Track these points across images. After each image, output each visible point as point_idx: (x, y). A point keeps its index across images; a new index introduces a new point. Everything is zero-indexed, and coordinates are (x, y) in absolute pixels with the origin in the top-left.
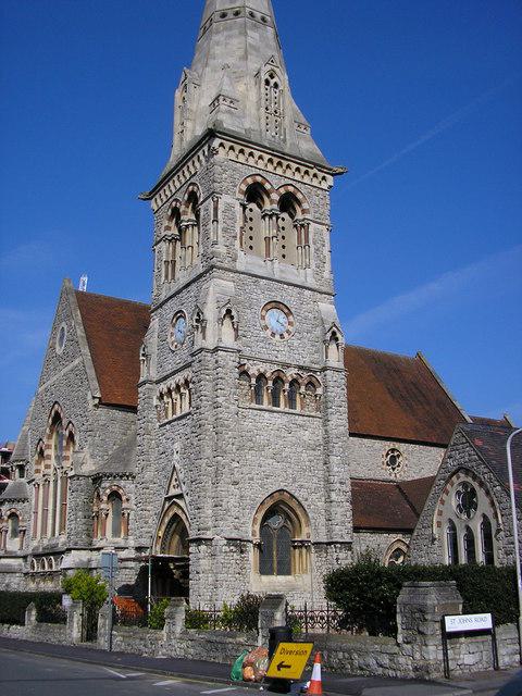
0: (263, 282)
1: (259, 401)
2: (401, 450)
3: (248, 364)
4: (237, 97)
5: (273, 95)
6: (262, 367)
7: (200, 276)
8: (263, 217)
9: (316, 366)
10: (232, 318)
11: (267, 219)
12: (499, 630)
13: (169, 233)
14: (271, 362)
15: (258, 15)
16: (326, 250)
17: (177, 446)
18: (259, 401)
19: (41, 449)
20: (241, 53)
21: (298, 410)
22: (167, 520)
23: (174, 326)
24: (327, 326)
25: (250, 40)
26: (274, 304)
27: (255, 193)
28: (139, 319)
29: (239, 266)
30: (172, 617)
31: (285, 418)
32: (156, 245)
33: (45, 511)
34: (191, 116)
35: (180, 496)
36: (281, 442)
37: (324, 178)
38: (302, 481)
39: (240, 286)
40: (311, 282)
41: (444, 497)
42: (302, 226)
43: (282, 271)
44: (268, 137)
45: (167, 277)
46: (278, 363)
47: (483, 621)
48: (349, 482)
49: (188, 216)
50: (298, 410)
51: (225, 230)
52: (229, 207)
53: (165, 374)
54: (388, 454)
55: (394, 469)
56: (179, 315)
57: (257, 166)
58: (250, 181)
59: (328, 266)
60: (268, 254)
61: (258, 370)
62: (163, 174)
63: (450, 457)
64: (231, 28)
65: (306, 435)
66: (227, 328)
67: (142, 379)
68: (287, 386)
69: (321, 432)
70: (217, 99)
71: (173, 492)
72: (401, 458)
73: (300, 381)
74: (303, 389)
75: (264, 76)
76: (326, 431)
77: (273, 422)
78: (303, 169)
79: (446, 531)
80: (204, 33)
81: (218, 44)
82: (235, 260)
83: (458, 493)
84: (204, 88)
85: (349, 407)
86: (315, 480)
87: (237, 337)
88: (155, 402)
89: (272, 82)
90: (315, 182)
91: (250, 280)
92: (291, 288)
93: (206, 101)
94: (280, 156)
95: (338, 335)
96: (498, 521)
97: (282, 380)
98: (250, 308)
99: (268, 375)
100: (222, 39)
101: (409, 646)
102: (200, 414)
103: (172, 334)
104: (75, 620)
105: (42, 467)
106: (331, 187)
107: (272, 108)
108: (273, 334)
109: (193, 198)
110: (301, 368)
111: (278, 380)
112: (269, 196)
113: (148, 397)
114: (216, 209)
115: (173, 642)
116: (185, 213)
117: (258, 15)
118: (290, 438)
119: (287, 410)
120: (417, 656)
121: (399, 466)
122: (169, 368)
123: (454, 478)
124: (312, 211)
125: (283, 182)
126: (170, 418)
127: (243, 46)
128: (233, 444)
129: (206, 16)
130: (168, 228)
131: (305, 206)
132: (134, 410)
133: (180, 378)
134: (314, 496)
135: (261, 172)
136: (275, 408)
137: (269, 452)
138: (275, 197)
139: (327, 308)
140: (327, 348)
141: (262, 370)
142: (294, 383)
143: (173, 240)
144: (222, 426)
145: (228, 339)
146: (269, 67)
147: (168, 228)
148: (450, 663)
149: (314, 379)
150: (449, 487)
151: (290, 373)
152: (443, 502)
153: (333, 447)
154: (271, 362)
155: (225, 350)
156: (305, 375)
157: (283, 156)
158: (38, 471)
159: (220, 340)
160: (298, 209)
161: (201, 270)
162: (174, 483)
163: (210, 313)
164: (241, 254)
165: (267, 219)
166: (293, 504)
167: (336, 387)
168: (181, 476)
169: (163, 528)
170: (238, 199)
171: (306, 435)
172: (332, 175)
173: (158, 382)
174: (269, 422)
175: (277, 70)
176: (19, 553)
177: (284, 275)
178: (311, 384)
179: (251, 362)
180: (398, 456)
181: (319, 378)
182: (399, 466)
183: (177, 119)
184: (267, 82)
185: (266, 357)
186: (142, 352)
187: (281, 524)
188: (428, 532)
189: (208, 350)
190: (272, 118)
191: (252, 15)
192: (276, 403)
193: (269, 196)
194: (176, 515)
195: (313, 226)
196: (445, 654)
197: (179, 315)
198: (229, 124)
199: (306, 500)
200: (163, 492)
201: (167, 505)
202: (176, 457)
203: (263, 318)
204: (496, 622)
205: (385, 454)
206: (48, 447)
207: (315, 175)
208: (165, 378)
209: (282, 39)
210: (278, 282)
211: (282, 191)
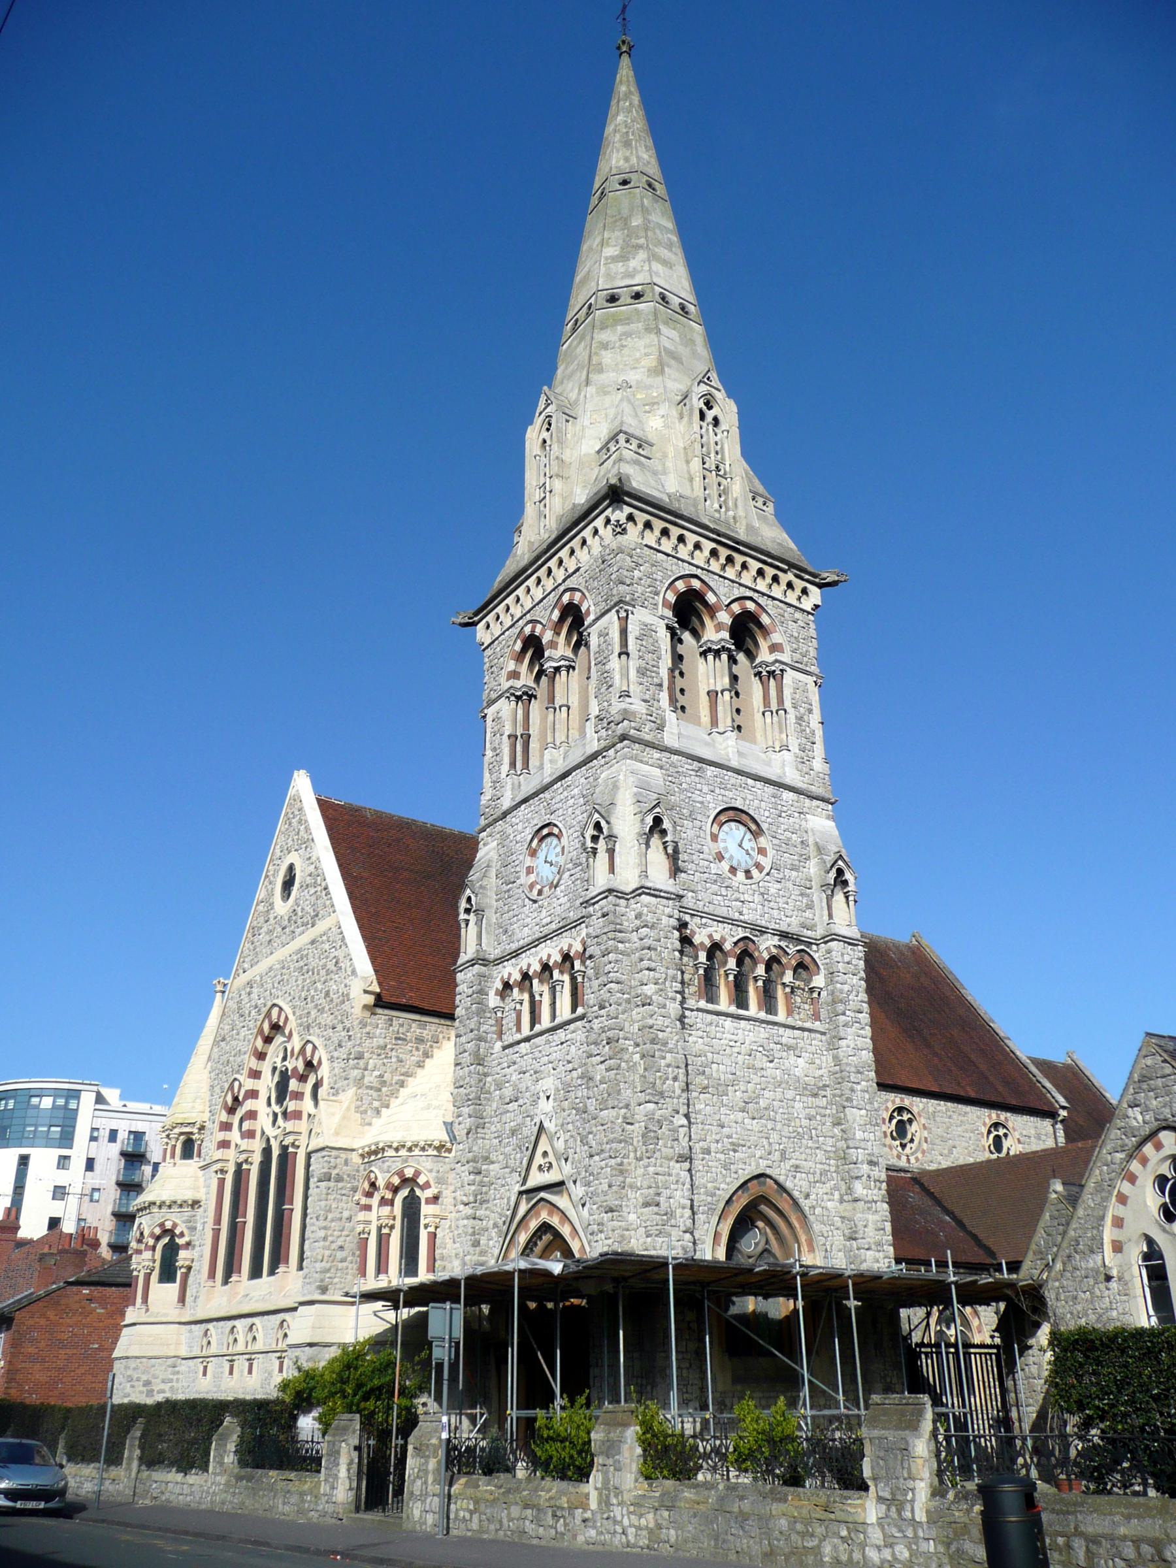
0: (710, 771)
1: (712, 999)
2: (915, 1110)
3: (693, 923)
4: (651, 437)
5: (713, 439)
6: (719, 932)
7: (594, 756)
8: (704, 654)
9: (809, 933)
10: (664, 832)
11: (710, 657)
13: (518, 684)
14: (733, 922)
15: (675, 301)
16: (815, 718)
18: (712, 999)
20: (651, 362)
21: (781, 1016)
22: (523, 1238)
23: (533, 853)
24: (829, 859)
25: (667, 344)
26: (731, 813)
27: (688, 609)
29: (669, 738)
30: (612, 1448)
31: (762, 1032)
32: (489, 706)
34: (561, 464)
35: (557, 1186)
36: (756, 1079)
37: (804, 591)
38: (796, 1158)
39: (673, 775)
40: (792, 776)
41: (1125, 1187)
42: (771, 674)
43: (740, 754)
44: (709, 511)
45: (513, 764)
46: (744, 925)
49: (558, 650)
50: (781, 1016)
51: (642, 672)
52: (647, 631)
53: (514, 946)
54: (891, 1118)
55: (903, 1146)
56: (545, 832)
57: (693, 558)
58: (681, 586)
59: (819, 750)
60: (714, 722)
61: (710, 936)
62: (497, 584)
64: (627, 320)
65: (799, 1066)
66: (657, 858)
68: (761, 970)
69: (827, 1060)
70: (614, 438)
71: (537, 1179)
73: (784, 960)
74: (788, 977)
76: (835, 1058)
77: (740, 1038)
78: (770, 572)
80: (574, 330)
81: (605, 346)
82: (661, 728)
83: (1162, 1180)
84: (585, 420)
86: (820, 1155)
87: (676, 870)
88: (493, 1000)
89: (710, 415)
90: (792, 598)
91: (688, 766)
92: (759, 784)
93: (590, 445)
94: (732, 546)
95: (848, 876)
97: (751, 956)
98: (692, 817)
99: (727, 946)
100: (614, 338)
103: (530, 870)
105: (234, 1136)
106: (817, 606)
107: (711, 463)
108: (733, 870)
109: (573, 617)
110: (784, 935)
111: (745, 956)
112: (712, 617)
114: (624, 632)
115: (617, 1512)
116: (553, 645)
117: (675, 301)
118: (771, 1070)
119: (762, 1015)
121: (912, 1141)
122: (524, 935)
123: (1148, 1149)
124: (787, 648)
125: (738, 592)
127: (654, 350)
129: (578, 300)
130: (515, 675)
131: (776, 638)
132: (451, 1017)
133: (551, 952)
134: (821, 1189)
135: (699, 572)
136: (741, 1012)
137: (736, 1097)
138: (725, 618)
139: (821, 824)
140: (829, 899)
141: (717, 937)
142: (772, 962)
144: (653, 1042)
145: (659, 876)
146: (704, 388)
147: (515, 675)
149: (807, 959)
150: (1135, 1166)
151: (767, 945)
152: (1123, 1199)
153: (852, 1090)
154: (733, 922)
155: (655, 893)
156: (792, 949)
157: (737, 546)
159: (644, 874)
160: (764, 645)
161: (595, 746)
162: (538, 1160)
163: (627, 824)
164: (671, 717)
165: (710, 657)
166: (784, 1204)
170: (662, 617)
171: (799, 1066)
172: (820, 586)
173: (500, 960)
174: (729, 1038)
177: (744, 761)
178: (803, 967)
179: (697, 920)
180: (910, 1121)
181: (816, 956)
183: (531, 478)
184: (702, 416)
185: (723, 911)
187: (760, 1248)
188: (1094, 1261)
190: (712, 477)
191: (663, 298)
193: (712, 617)
194: (545, 1228)
195: (790, 676)
197: (545, 832)
198: (639, 482)
199: (807, 1196)
200: (516, 1177)
201: (523, 1208)
202: (545, 1106)
203: (714, 838)
205: (887, 1116)
207: (790, 585)
208: (515, 954)
209: (714, 340)
210: (739, 772)
211: (736, 608)
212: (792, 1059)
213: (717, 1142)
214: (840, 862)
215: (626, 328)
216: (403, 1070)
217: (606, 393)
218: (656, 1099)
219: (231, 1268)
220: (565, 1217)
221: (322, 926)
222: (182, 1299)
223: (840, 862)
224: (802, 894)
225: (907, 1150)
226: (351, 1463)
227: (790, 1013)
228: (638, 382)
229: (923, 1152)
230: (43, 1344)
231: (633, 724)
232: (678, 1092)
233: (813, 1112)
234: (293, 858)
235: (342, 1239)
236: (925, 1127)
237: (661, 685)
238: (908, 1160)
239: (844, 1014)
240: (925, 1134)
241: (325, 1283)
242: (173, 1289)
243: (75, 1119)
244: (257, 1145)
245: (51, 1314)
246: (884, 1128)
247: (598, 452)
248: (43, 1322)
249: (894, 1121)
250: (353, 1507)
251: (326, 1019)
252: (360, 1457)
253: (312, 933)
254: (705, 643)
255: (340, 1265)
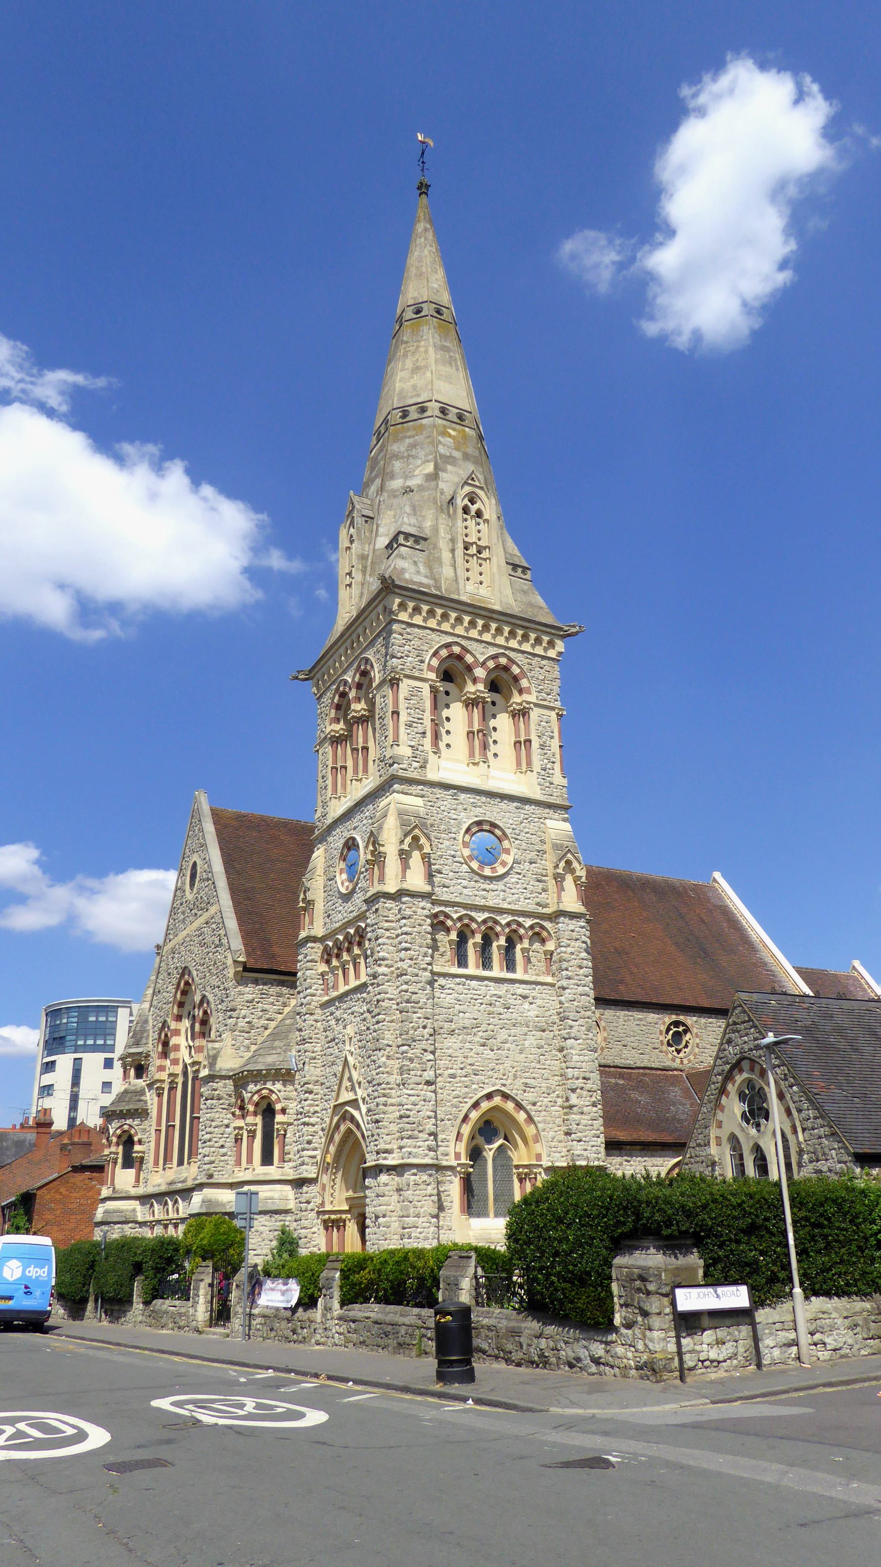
12: (762, 1315)
16: (555, 744)
17: (350, 1030)
19: (166, 1035)
21: (519, 975)
22: (337, 1138)
27: (452, 672)
28: (302, 839)
33: (170, 1127)
35: (354, 1103)
47: (736, 1297)
48: (596, 1076)
55: (678, 1051)
63: (729, 1042)
67: (303, 934)
70: (395, 539)
71: (346, 1096)
72: (688, 1036)
75: (460, 502)
79: (728, 1152)
81: (396, 456)
85: (594, 968)
87: (430, 877)
89: (474, 508)
96: (797, 1138)
101: (630, 1332)
102: (378, 985)
104: (202, 1292)
113: (311, 965)
115: (329, 1324)
120: (640, 1346)
124: (533, 690)
125: (492, 651)
126: (343, 989)
128: (424, 1027)
138: (480, 673)
143: (336, 741)
144: (408, 1002)
146: (467, 489)
148: (686, 1357)
158: (161, 1068)
162: (346, 1083)
163: (391, 840)
167: (573, 941)
168: (355, 1075)
169: (332, 1149)
172: (562, 637)
174: (468, 994)
175: (481, 493)
176: (133, 1192)
180: (686, 1031)
182: (686, 1046)
184: (466, 510)
186: (302, 896)
189: (387, 896)
192: (486, 963)
195: (535, 714)
196: (679, 1344)
204: (758, 1302)
205: (663, 1028)
206: (177, 1032)
212: (526, 1006)
213: (462, 1069)
214: (569, 855)
215: (411, 440)
216: (267, 1016)
217: (395, 497)
218: (409, 1042)
219: (167, 1159)
220: (358, 1126)
221: (213, 910)
222: (137, 1180)
223: (569, 855)
224: (538, 881)
225: (682, 1055)
226: (206, 1294)
227: (526, 971)
228: (419, 486)
229: (695, 1055)
230: (58, 1212)
231: (401, 766)
232: (427, 1036)
233: (543, 1042)
234: (195, 858)
235: (223, 1139)
236: (697, 1036)
237: (424, 733)
238: (682, 1062)
239: (567, 969)
240: (698, 1041)
241: (210, 1172)
242: (132, 1172)
243: (115, 1029)
244: (178, 1069)
245: (63, 1190)
246: (662, 1038)
247: (387, 547)
248: (58, 1196)
249: (671, 1032)
250: (208, 1323)
251: (215, 981)
252: (212, 1291)
253: (206, 916)
254: (465, 694)
255: (223, 1158)
